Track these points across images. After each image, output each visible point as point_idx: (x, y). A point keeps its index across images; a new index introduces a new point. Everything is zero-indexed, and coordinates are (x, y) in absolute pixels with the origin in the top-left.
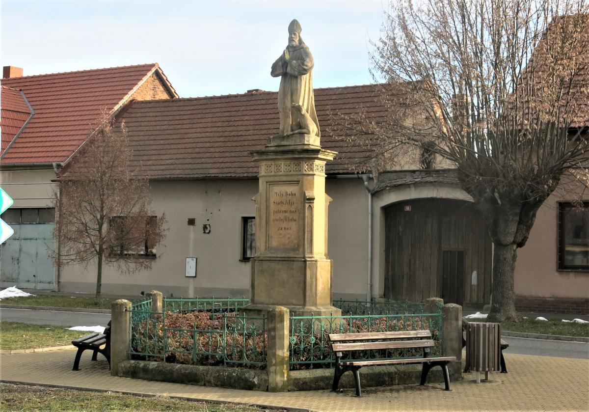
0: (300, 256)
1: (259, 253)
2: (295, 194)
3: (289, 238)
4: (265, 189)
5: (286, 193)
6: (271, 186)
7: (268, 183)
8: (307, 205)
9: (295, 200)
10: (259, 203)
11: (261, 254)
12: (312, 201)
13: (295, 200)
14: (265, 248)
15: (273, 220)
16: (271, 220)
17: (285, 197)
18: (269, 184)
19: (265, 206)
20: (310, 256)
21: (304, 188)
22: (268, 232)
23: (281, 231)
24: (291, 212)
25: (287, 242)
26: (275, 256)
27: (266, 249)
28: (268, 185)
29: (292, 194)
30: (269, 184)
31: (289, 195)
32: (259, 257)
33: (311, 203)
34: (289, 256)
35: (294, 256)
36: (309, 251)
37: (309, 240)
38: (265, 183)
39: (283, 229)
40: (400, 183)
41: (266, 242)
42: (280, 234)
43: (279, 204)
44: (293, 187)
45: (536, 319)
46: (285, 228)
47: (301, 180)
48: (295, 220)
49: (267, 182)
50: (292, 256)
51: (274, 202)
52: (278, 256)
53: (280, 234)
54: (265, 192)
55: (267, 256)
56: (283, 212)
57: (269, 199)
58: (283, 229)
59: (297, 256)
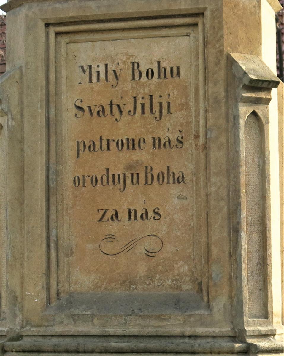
0: (217, 330)
1: (18, 320)
2: (175, 72)
3: (149, 254)
4: (184, 31)
5: (135, 66)
6: (64, 40)
7: (52, 30)
8: (244, 110)
9: (175, 93)
10: (15, 111)
11: (27, 322)
12: (263, 95)
13: (175, 93)
14: (44, 295)
15: (76, 181)
16: (68, 180)
17: (129, 85)
18: (58, 34)
19: (41, 121)
20: (263, 329)
21: (228, 40)
22: (53, 232)
23: (112, 227)
24: (157, 143)
25: (142, 269)
26: (95, 330)
27: (49, 301)
28: (52, 36)
29: (163, 73)
30: (58, 34)
31: (150, 74)
32: (19, 337)
33: (258, 101)
34: (161, 331)
35: (188, 331)
36: (256, 309)
37: (255, 258)
38: (41, 25)
39: (124, 216)
40: (206, 61)
41: (48, 274)
42: (111, 238)
43: (101, 112)
44: (165, 42)
45: (242, 231)
46: (132, 214)
47: (210, 7)
48: (180, 180)
49: (47, 25)
50: (177, 331)
51: (80, 108)
52: (111, 330)
53: (111, 238)
54: (41, 65)
55: (58, 329)
56: (120, 145)
57: (58, 94)
58: (124, 216)
59: (200, 330)
